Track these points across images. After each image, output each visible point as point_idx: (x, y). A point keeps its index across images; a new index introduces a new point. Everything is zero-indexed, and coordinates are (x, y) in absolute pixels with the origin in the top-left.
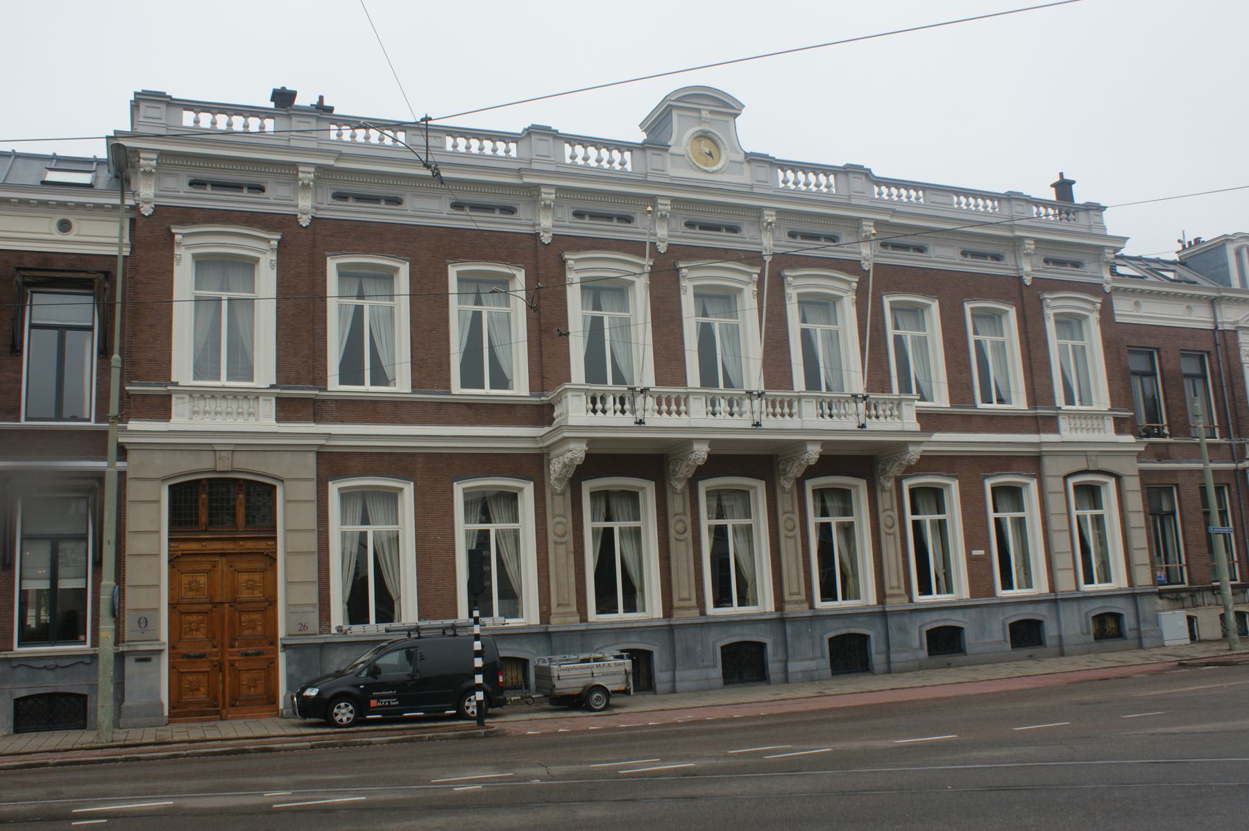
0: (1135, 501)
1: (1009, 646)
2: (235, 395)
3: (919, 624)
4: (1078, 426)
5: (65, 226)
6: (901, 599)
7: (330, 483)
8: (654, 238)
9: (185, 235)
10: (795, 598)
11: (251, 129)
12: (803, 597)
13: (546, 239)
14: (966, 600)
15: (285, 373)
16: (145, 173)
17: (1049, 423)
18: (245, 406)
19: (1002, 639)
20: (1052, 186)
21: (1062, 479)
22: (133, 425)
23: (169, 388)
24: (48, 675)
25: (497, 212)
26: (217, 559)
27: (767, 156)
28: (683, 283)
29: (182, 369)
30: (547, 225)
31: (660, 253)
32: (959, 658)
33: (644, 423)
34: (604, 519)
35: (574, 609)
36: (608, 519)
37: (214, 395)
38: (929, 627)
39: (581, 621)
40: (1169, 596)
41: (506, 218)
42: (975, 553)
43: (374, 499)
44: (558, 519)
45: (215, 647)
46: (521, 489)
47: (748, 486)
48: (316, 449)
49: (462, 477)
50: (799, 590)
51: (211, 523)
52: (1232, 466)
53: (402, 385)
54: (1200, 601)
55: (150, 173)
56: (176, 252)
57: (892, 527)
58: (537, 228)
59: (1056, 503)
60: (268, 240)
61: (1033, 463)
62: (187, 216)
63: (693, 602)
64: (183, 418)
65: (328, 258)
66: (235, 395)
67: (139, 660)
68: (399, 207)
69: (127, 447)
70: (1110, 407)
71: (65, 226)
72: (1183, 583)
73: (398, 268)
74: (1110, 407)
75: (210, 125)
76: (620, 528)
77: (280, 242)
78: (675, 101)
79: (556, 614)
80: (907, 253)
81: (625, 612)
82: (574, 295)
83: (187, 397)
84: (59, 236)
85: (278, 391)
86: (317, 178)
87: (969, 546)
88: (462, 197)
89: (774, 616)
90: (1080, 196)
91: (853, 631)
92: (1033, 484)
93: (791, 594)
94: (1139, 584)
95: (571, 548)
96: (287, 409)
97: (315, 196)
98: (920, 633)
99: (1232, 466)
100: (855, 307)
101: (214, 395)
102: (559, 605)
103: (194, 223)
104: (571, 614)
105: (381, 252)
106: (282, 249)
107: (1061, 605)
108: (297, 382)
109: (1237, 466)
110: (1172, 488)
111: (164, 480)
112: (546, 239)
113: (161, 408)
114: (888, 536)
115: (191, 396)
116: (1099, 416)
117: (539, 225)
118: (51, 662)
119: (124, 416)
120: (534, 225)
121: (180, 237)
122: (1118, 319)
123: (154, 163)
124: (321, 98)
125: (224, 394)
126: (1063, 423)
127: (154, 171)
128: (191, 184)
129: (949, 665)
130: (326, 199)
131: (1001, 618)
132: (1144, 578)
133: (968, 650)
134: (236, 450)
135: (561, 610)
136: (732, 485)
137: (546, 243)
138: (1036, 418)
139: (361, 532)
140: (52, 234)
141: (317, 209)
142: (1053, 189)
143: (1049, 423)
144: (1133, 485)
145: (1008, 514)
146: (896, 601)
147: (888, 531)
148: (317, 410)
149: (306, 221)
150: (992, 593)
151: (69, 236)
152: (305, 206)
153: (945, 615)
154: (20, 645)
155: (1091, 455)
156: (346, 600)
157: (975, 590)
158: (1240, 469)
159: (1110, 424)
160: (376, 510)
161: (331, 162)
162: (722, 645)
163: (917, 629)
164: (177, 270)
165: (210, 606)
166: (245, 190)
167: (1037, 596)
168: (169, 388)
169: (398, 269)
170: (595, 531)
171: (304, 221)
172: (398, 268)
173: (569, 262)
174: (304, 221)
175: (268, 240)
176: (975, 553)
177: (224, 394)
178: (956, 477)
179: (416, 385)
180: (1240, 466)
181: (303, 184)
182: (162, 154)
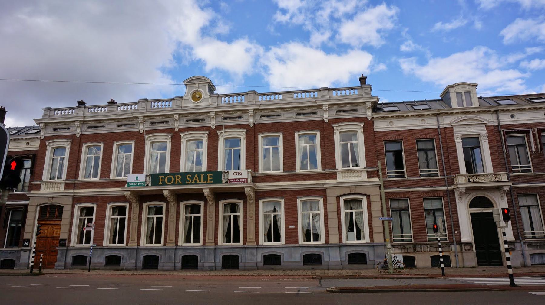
0: (376, 206)
1: (347, 263)
2: (354, 171)
3: (262, 252)
4: (51, 187)
5: (28, 144)
6: (253, 243)
7: (298, 199)
8: (249, 122)
9: (336, 127)
10: (210, 241)
11: (307, 97)
12: (213, 241)
13: (326, 121)
14: (284, 245)
15: (68, 176)
16: (325, 111)
17: (333, 176)
18: (358, 174)
19: (300, 261)
20: (78, 102)
21: (336, 198)
22: (32, 192)
23: (336, 171)
24: (9, 255)
25: (352, 112)
26: (49, 226)
27: (327, 88)
28: (146, 142)
29: (45, 177)
30: (326, 117)
31: (176, 131)
32: (278, 267)
33: (149, 185)
34: (117, 214)
35: (136, 242)
36: (351, 209)
37: (348, 171)
38: (305, 254)
39: (215, 245)
40: (398, 247)
41: (355, 113)
42: (290, 227)
43: (316, 204)
44: (251, 212)
45: (46, 249)
46: (363, 199)
47: (361, 198)
48: (355, 187)
49: (110, 202)
50: (253, 237)
51: (50, 216)
52: (445, 188)
53: (319, 169)
54: (419, 249)
55: (326, 111)
56: (334, 132)
57: (252, 217)
58: (323, 118)
59: (332, 207)
60: (360, 125)
61: (322, 192)
62: (149, 132)
63: (174, 241)
64: (340, 178)
65: (259, 135)
66: (354, 171)
67: (24, 252)
68: (316, 115)
69: (30, 198)
70: (366, 167)
71: (512, 117)
72: (412, 241)
73: (317, 134)
74: (366, 167)
75: (274, 99)
76: (312, 213)
77: (364, 125)
78: (187, 82)
79: (207, 242)
80: (199, 122)
81: (313, 241)
82: (337, 138)
83: (341, 173)
84: (512, 119)
85: (367, 169)
86: (179, 117)
87: (287, 223)
88: (225, 116)
89: (202, 247)
90: (3, 107)
91: (232, 254)
92: (322, 200)
93: (209, 240)
94: (375, 241)
95: (137, 223)
96: (68, 186)
97: (254, 118)
98: (261, 256)
99: (445, 188)
100: (245, 140)
101: (348, 171)
102: (131, 240)
103: (339, 123)
104: (135, 243)
105: (125, 140)
106: (72, 143)
107: (177, 250)
108: (372, 166)
109: (447, 188)
110: (441, 198)
111: (37, 206)
112: (326, 121)
113: (38, 187)
114: (250, 220)
115: (342, 172)
116: (360, 171)
117: (324, 117)
118: (9, 252)
119: (30, 190)
120: (322, 117)
121: (220, 134)
122: (375, 130)
123: (214, 114)
124: (112, 99)
125: (351, 171)
126: (339, 176)
127: (327, 110)
128: (297, 115)
129: (272, 269)
130: (258, 118)
131: (300, 252)
132: (379, 238)
133: (282, 263)
134: (53, 197)
135: (132, 242)
136: (349, 198)
137: (370, 120)
138: (325, 174)
139: (351, 212)
140: (543, 117)
141: (255, 121)
142: (78, 103)
143: (333, 176)
144: (375, 199)
145: (272, 213)
146: (250, 244)
147: (250, 218)
148: (74, 186)
149: (213, 128)
150: (297, 242)
151: (29, 146)
152: (251, 121)
153: (273, 250)
154: (6, 247)
155: (352, 187)
156: (305, 232)
157: (287, 242)
158: (449, 189)
159: (365, 174)
160: (354, 205)
161: (258, 107)
162: (348, 254)
163: (260, 254)
164: (47, 152)
165: (46, 238)
166: (156, 123)
167: (322, 244)
168: (336, 171)
169: (316, 134)
170: (346, 214)
171: (252, 125)
172: (317, 134)
173: (181, 136)
174: (252, 125)
175: (360, 125)
176: (290, 227)
177: (351, 171)
178: (283, 198)
179: (285, 170)
180: (450, 188)
181: (140, 122)
182: (329, 105)
